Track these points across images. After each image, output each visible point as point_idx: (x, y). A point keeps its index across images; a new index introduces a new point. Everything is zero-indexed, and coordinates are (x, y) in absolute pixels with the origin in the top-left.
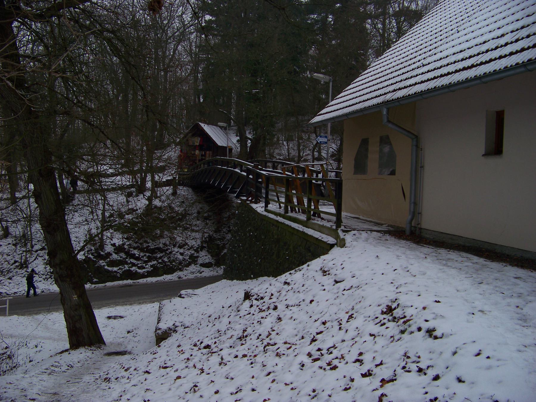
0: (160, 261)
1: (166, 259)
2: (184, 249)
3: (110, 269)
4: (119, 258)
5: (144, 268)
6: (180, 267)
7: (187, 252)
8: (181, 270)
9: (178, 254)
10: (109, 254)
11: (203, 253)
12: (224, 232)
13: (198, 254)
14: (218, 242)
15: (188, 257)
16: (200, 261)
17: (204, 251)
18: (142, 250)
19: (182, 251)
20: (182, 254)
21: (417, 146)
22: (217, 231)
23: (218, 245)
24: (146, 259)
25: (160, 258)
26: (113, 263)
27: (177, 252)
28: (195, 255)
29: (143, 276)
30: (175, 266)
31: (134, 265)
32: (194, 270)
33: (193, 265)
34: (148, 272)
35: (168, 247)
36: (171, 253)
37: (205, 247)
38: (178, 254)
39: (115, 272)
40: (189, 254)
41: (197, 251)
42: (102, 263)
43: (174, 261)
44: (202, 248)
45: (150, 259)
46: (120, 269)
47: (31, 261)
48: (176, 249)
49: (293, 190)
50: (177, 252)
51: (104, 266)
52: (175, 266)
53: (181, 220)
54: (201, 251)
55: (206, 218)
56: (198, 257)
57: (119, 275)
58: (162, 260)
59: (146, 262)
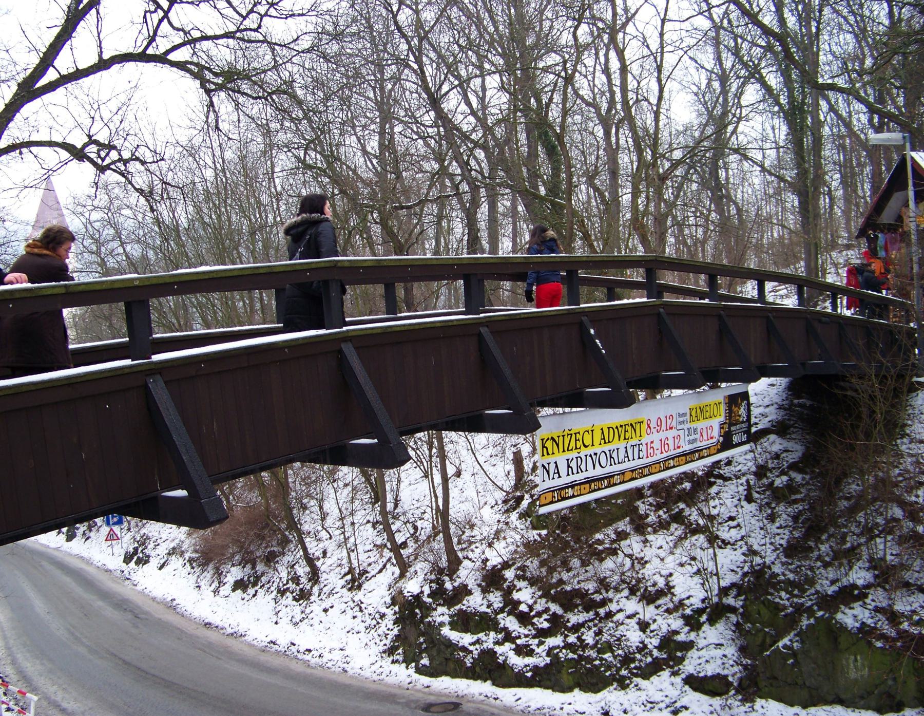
0: (572, 639)
1: (589, 638)
2: (657, 607)
3: (454, 636)
4: (484, 609)
5: (530, 653)
6: (624, 672)
7: (660, 620)
8: (623, 685)
9: (633, 622)
10: (463, 591)
11: (711, 634)
12: (819, 558)
13: (692, 636)
14: (782, 598)
15: (655, 642)
16: (690, 666)
17: (720, 626)
18: (546, 590)
19: (649, 612)
20: (644, 626)
21: (125, 662)
22: (792, 550)
23: (777, 608)
24: (546, 625)
25: (576, 628)
26: (464, 621)
27: (629, 617)
28: (681, 638)
29: (519, 680)
30: (609, 667)
31: (508, 637)
32: (658, 697)
33: (665, 674)
34: (535, 669)
35: (611, 594)
36: (609, 615)
37: (733, 610)
38: (633, 622)
39: (464, 649)
40: (665, 629)
41: (693, 623)
42: (441, 615)
43: (609, 647)
44: (716, 612)
45: (557, 625)
46: (478, 641)
47: (373, 573)
48: (632, 605)
49: (532, 676)
50: (629, 617)
51: (442, 624)
52: (609, 667)
53: (690, 498)
54: (712, 621)
55: (779, 495)
56: (688, 646)
57: (468, 661)
58: (579, 638)
59: (542, 634)
